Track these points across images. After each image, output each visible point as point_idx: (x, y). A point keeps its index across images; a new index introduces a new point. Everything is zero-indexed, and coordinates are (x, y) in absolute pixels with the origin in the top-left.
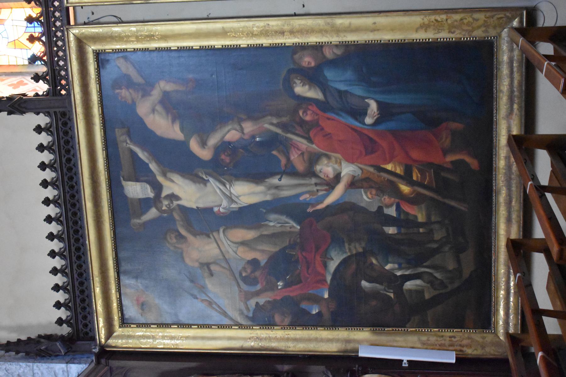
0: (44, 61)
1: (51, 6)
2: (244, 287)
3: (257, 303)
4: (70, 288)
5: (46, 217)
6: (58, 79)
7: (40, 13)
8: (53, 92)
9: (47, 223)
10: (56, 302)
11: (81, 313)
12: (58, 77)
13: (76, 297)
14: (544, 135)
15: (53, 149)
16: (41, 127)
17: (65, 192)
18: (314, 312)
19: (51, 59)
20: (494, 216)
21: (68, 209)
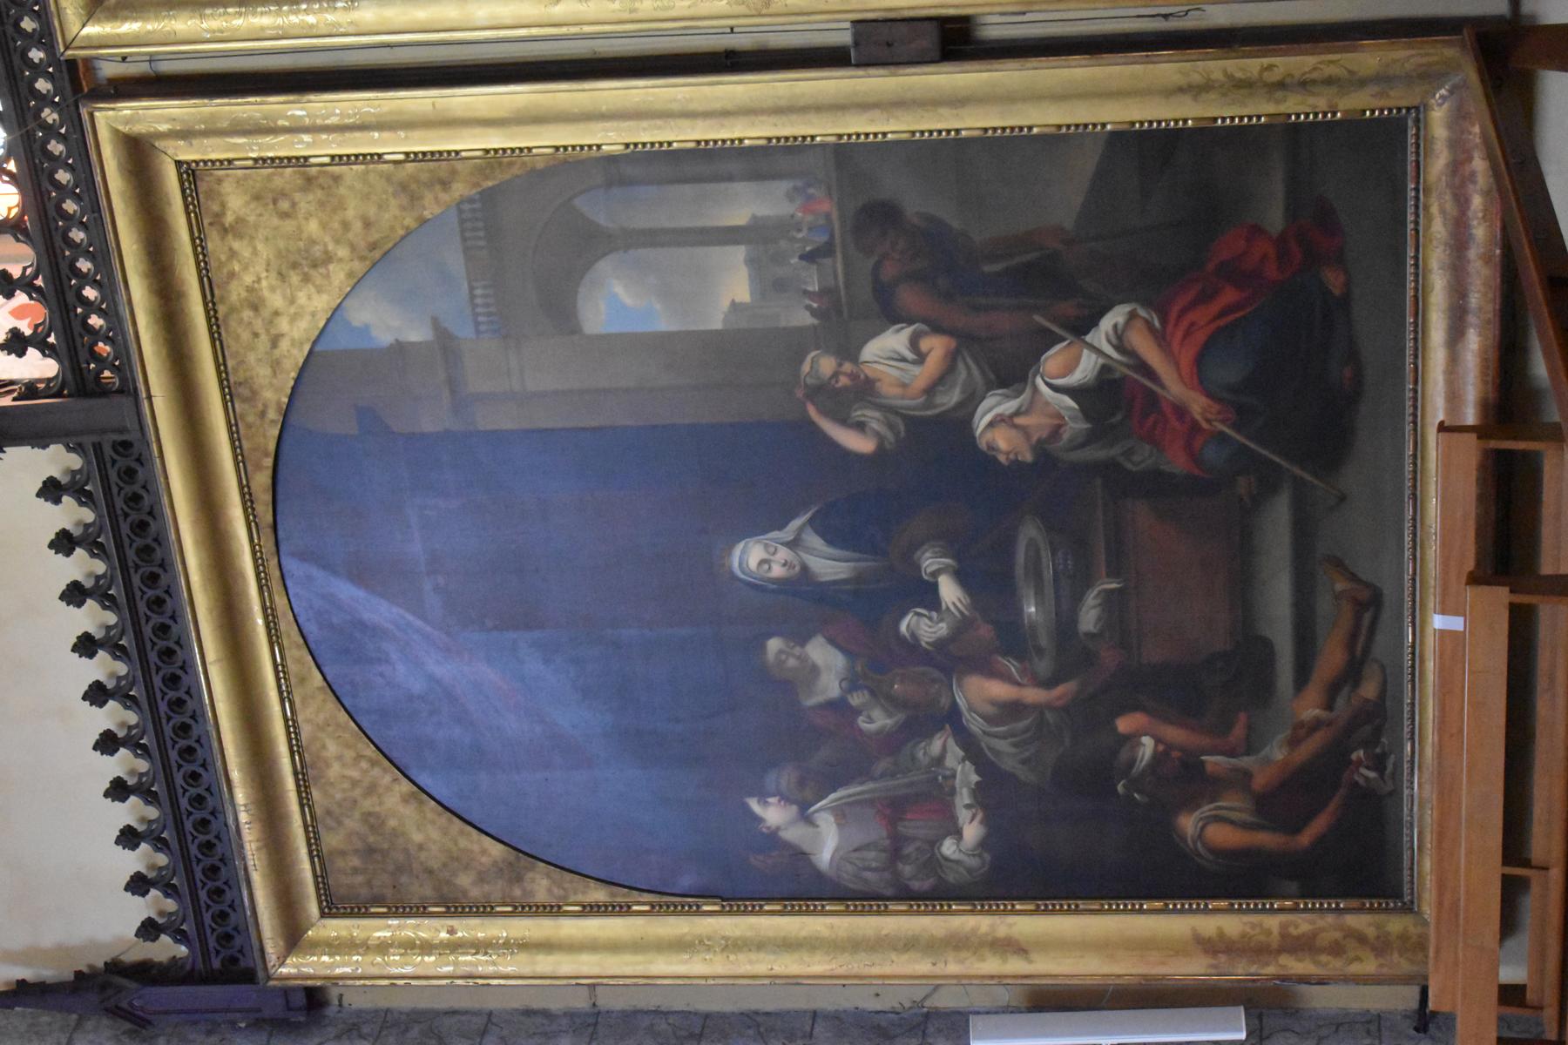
0: (38, 290)
4: (130, 642)
6: (15, 48)
7: (18, 205)
10: (57, 534)
11: (126, 515)
12: (71, 280)
13: (116, 516)
14: (1556, 223)
19: (69, 332)
20: (1409, 885)
21: (194, 859)
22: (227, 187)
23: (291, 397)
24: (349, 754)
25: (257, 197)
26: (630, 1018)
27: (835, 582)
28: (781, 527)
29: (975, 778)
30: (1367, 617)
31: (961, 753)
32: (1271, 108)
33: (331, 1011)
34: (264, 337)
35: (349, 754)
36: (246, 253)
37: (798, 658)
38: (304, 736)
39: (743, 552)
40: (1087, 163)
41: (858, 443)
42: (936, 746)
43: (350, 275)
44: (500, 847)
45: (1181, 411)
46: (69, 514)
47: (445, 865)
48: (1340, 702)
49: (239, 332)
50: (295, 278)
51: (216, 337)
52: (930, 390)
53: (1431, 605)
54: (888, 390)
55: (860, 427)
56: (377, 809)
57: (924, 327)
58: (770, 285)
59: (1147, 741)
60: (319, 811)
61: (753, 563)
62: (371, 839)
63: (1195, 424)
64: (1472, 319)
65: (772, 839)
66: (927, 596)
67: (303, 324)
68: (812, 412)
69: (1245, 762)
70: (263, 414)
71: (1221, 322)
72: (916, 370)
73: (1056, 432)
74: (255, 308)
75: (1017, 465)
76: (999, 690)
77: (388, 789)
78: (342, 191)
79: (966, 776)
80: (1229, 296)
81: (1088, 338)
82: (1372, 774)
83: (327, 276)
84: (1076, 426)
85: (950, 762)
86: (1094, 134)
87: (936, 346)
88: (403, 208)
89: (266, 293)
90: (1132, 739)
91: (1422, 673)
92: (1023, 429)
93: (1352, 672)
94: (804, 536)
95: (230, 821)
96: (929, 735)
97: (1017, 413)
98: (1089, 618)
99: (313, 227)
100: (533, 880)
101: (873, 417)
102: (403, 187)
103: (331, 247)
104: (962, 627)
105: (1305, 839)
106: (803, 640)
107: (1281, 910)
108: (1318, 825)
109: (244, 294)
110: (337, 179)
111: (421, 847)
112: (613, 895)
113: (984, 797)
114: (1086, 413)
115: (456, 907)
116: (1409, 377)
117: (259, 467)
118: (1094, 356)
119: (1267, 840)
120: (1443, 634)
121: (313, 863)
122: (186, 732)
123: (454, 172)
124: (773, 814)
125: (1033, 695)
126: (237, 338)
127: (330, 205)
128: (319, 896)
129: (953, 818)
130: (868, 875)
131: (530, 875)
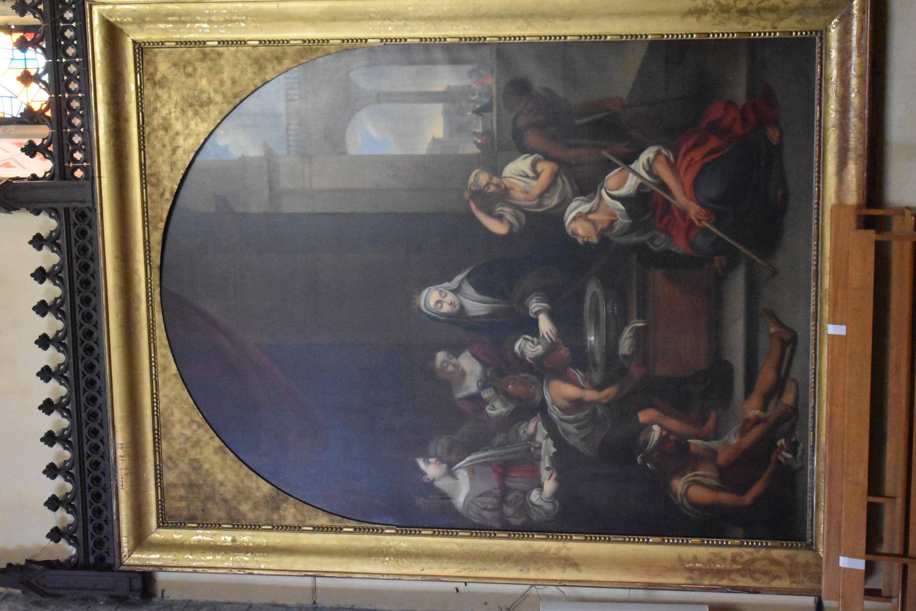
1: (64, 90)
5: (34, 237)
8: (62, 172)
9: (48, 477)
11: (78, 258)
15: (61, 277)
16: (48, 337)
17: (74, 292)
22: (159, 58)
25: (175, 65)
27: (478, 317)
29: (553, 450)
30: (788, 350)
32: (739, 28)
34: (169, 148)
36: (165, 97)
37: (454, 365)
38: (161, 406)
40: (635, 61)
41: (498, 228)
42: (532, 426)
43: (221, 112)
44: (269, 486)
45: (684, 213)
46: (55, 390)
47: (234, 496)
48: (771, 406)
50: (190, 113)
51: (142, 148)
52: (541, 196)
54: (517, 195)
55: (500, 218)
56: (198, 457)
57: (541, 157)
58: (456, 128)
59: (656, 428)
60: (164, 456)
61: (432, 302)
64: (852, 155)
65: (430, 487)
66: (531, 328)
67: (191, 141)
68: (473, 206)
69: (713, 444)
70: (162, 195)
72: (534, 183)
74: (166, 129)
76: (570, 391)
77: (207, 443)
78: (222, 62)
79: (548, 448)
80: (713, 143)
82: (789, 456)
83: (208, 113)
84: (623, 221)
85: (539, 438)
87: (546, 168)
88: (255, 73)
89: (173, 121)
90: (647, 426)
92: (593, 222)
93: (778, 388)
96: (528, 420)
97: (590, 212)
98: (625, 346)
99: (204, 83)
100: (286, 509)
101: (507, 211)
102: (256, 61)
103: (212, 95)
104: (551, 348)
105: (748, 499)
108: (757, 489)
109: (161, 121)
110: (220, 55)
111: (222, 484)
112: (332, 521)
114: (630, 212)
115: (237, 524)
117: (156, 228)
118: (635, 178)
119: (726, 498)
120: (832, 337)
122: (85, 253)
123: (284, 53)
124: (432, 469)
125: (590, 395)
126: (154, 147)
128: (158, 514)
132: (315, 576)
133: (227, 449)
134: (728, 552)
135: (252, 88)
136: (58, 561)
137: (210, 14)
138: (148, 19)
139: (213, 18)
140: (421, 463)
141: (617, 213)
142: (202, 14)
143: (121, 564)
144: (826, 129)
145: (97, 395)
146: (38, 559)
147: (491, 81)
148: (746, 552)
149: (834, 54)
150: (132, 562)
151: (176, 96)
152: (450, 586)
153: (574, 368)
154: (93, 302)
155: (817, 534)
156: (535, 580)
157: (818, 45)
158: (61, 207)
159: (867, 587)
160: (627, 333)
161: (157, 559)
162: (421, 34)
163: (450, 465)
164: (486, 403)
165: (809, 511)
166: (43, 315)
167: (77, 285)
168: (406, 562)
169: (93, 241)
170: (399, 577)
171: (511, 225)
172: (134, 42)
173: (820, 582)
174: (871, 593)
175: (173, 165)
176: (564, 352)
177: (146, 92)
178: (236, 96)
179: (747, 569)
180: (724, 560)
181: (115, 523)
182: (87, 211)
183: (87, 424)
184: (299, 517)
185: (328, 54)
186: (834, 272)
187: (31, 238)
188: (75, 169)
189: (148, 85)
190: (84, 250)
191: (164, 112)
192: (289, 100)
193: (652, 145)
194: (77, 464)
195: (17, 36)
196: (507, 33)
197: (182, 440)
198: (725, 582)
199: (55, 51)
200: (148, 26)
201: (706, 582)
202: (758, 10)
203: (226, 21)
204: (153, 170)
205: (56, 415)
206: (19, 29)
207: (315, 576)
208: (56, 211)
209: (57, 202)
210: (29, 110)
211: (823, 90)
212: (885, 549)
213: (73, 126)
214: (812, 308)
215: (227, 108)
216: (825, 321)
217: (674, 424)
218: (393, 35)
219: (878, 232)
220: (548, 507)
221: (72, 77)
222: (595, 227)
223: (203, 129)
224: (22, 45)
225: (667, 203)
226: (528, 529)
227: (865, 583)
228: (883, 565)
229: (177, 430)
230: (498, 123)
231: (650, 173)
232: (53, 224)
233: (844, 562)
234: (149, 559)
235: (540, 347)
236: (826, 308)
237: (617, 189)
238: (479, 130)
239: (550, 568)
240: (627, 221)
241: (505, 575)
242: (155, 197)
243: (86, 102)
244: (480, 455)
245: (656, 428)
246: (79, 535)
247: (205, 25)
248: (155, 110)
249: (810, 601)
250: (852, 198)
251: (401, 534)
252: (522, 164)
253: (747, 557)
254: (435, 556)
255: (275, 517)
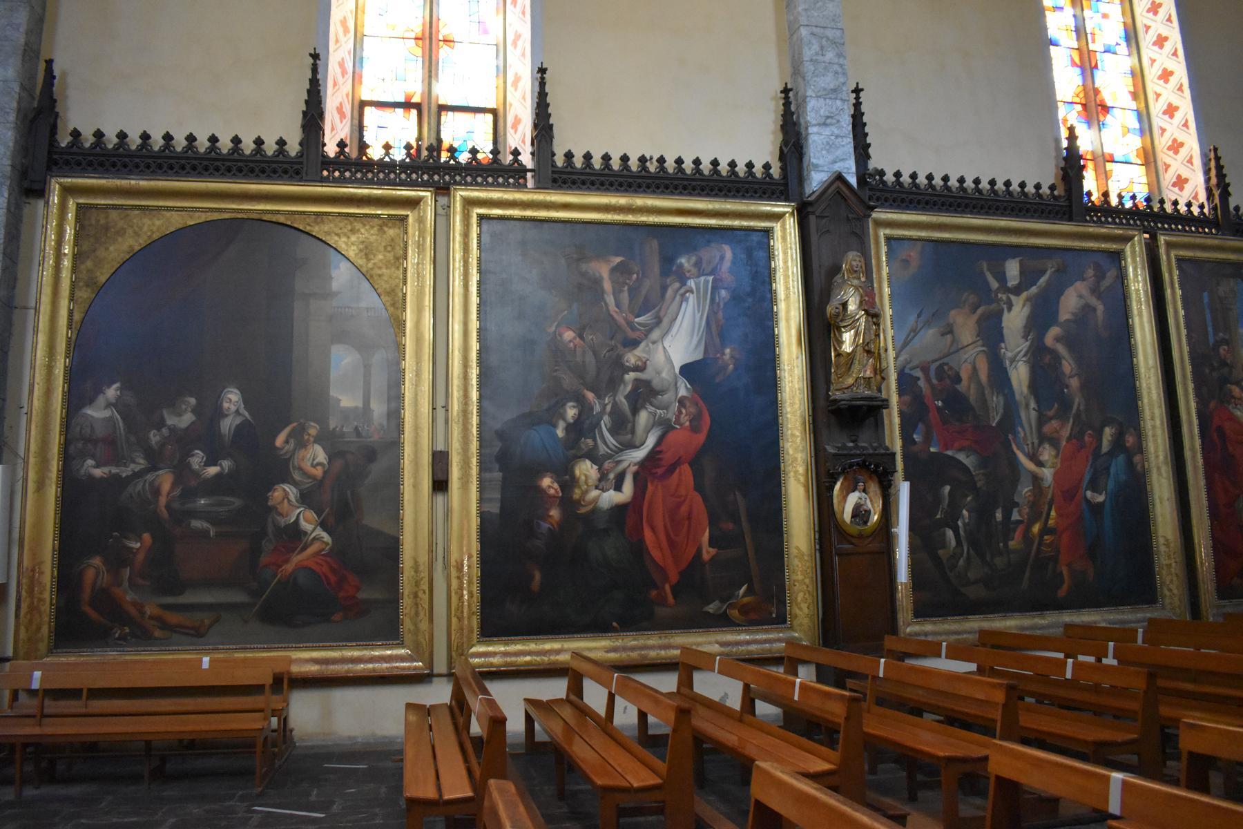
2: (933, 367)
3: (919, 379)
8: (327, 163)
18: (915, 436)
22: (397, 231)
23: (314, 237)
24: (155, 229)
25: (392, 240)
26: (9, 322)
27: (220, 428)
28: (245, 408)
29: (124, 475)
30: (192, 632)
31: (136, 470)
32: (406, 593)
33: (24, 198)
34: (340, 231)
35: (155, 229)
36: (372, 232)
37: (186, 409)
38: (164, 213)
39: (236, 393)
40: (388, 529)
41: (280, 441)
42: (142, 461)
43: (361, 266)
44: (104, 280)
45: (287, 561)
47: (97, 257)
48: (153, 622)
49: (345, 225)
50: (361, 246)
51: (340, 214)
52: (300, 469)
53: (217, 656)
54: (302, 453)
55: (287, 442)
56: (127, 234)
57: (326, 469)
58: (346, 414)
59: (139, 545)
60: (129, 212)
61: (230, 396)
62: (113, 230)
63: (280, 566)
64: (324, 667)
65: (99, 391)
66: (211, 462)
67: (344, 246)
68: (295, 424)
69: (126, 584)
70: (309, 225)
71: (323, 578)
72: (309, 464)
73: (281, 515)
74: (351, 230)
75: (267, 499)
76: (166, 487)
77: (137, 241)
78: (393, 269)
79: (125, 472)
80: (333, 579)
81: (318, 527)
82: (117, 635)
83: (361, 258)
84: (282, 522)
85: (132, 466)
86: (399, 531)
87: (318, 472)
88: (385, 289)
89: (357, 235)
90: (140, 539)
91: (166, 654)
92: (282, 502)
93: (165, 626)
94: (241, 417)
95: (133, 177)
96: (145, 458)
97: (289, 501)
98: (197, 524)
99: (380, 257)
100: (86, 291)
101: (291, 446)
102: (393, 290)
103: (372, 261)
104: (197, 474)
105: (87, 609)
106: (193, 411)
107: (51, 599)
108: (94, 615)
109: (357, 228)
110: (398, 268)
111: (107, 249)
112: (76, 323)
113: (115, 481)
114: (288, 526)
115: (77, 258)
116: (269, 646)
117: (287, 219)
118: (311, 529)
119: (86, 594)
120: (201, 661)
121: (104, 205)
123: (397, 308)
124: (112, 392)
125: (163, 500)
126: (340, 222)
127: (388, 265)
128: (87, 204)
129: (105, 465)
130: (78, 429)
131: (89, 290)
132: (36, 309)
133: (131, 254)
134: (47, 595)
135: (376, 287)
136: (56, 133)
137: (423, 264)
138: (422, 226)
139: (420, 266)
140: (115, 386)
141: (288, 518)
142: (423, 259)
143: (52, 176)
144: (341, 650)
145: (151, 170)
146: (59, 121)
147: (376, 438)
148: (46, 608)
149: (389, 652)
150: (52, 184)
151: (372, 239)
152: (25, 403)
153: (182, 489)
154: (170, 172)
155: (60, 656)
156: (28, 462)
157: (395, 642)
158: (304, 159)
159: (20, 692)
160: (206, 525)
161: (54, 201)
162: (407, 394)
163: (115, 405)
164: (159, 430)
165: (76, 650)
166: (232, 141)
167: (274, 165)
168: (44, 373)
169: (280, 178)
170: (33, 367)
171: (282, 449)
172: (407, 216)
173: (24, 659)
174: (15, 695)
175: (328, 233)
176: (194, 483)
177: (376, 220)
178: (372, 276)
179: (33, 609)
180: (41, 593)
181: (82, 175)
182: (300, 176)
183: (154, 162)
184: (80, 300)
185: (396, 336)
186: (245, 660)
187: (284, 138)
188: (328, 171)
189: (380, 222)
190: (275, 172)
191: (363, 231)
192: (367, 309)
193: (333, 540)
194: (125, 153)
195: (414, 145)
196: (406, 448)
197: (140, 225)
198: (24, 594)
199: (403, 166)
200: (417, 225)
201: (24, 581)
202: (416, 604)
203: (418, 274)
204: (326, 220)
205: (162, 142)
206: (419, 146)
207: (36, 309)
208: (302, 156)
209: (307, 158)
210: (367, 146)
211: (366, 647)
212: (47, 702)
213: (356, 172)
214: (221, 647)
215: (364, 270)
216: (212, 655)
217: (141, 557)
218: (407, 377)
219: (271, 686)
220: (82, 472)
221: (387, 175)
222: (279, 504)
223: (351, 253)
224: (408, 147)
225: (293, 551)
226: (67, 457)
227: (23, 690)
228: (35, 702)
229: (147, 221)
230: (349, 442)
231: (314, 539)
232: (293, 154)
233: (37, 674)
234: (54, 196)
235: (197, 467)
236: (221, 656)
237: (304, 518)
238: (345, 429)
239: (37, 473)
240: (283, 525)
241: (32, 441)
242: (308, 220)
243: (370, 183)
244: (121, 424)
245: (139, 545)
246: (75, 149)
247: (416, 261)
248: (365, 225)
249: (10, 653)
250: (295, 669)
251: (65, 370)
252: (321, 456)
253: (43, 608)
254: (48, 393)
255: (81, 284)
